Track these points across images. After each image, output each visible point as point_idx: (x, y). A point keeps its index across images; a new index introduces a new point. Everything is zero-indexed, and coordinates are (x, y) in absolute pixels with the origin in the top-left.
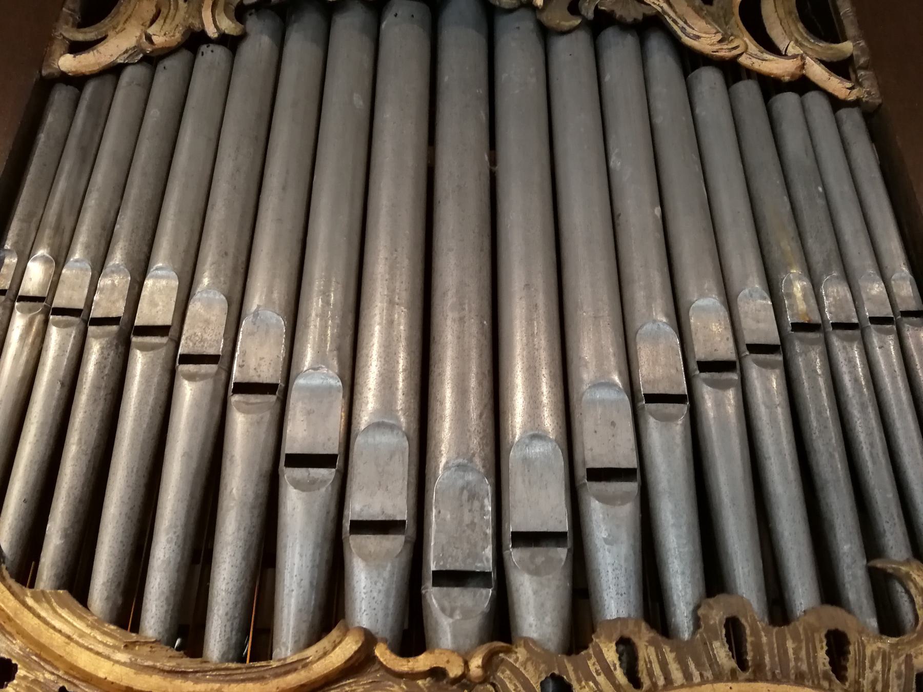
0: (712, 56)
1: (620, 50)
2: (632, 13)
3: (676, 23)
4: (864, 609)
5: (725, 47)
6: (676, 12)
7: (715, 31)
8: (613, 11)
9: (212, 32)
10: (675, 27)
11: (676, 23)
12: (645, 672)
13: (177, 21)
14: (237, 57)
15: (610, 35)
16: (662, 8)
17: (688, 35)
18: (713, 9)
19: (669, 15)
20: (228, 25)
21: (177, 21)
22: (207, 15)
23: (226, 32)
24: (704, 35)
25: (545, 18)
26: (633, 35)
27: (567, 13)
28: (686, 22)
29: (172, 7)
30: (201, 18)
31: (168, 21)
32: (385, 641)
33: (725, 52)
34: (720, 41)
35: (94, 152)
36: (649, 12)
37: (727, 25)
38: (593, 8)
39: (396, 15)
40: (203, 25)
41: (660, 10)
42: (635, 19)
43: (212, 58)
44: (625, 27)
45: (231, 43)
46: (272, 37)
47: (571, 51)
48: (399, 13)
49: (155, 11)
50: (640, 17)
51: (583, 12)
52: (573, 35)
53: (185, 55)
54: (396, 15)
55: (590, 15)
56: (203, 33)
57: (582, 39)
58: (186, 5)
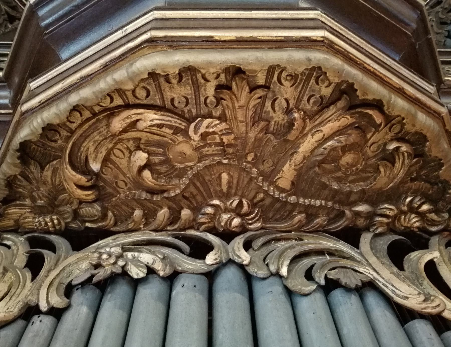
0: (422, 312)
1: (347, 305)
2: (352, 281)
3: (387, 287)
4: (151, 122)
5: (430, 305)
6: (383, 278)
7: (417, 293)
8: (339, 279)
9: (44, 307)
10: (386, 290)
11: (387, 287)
12: (129, 114)
13: (19, 299)
14: (60, 323)
15: (338, 295)
16: (372, 275)
17: (398, 296)
18: (407, 273)
19: (379, 281)
20: (57, 301)
21: (19, 299)
22: (43, 292)
23: (55, 306)
24: (410, 296)
25: (290, 284)
26: (355, 295)
27: (305, 280)
28: (393, 286)
29: (20, 287)
30: (38, 295)
31: (13, 298)
32: (112, 76)
33: (430, 308)
34: (424, 301)
35: (145, 11)
36: (365, 280)
37: (422, 286)
38: (323, 277)
39: (183, 286)
40: (38, 301)
41: (372, 277)
42: (356, 285)
43: (41, 325)
44: (348, 289)
45: (57, 313)
46: (90, 308)
47: (312, 308)
48: (185, 285)
49: (6, 290)
50: (360, 284)
51: (317, 280)
52: (312, 296)
53: (21, 323)
54: (183, 286)
55: (323, 282)
56: (37, 306)
57: (319, 297)
58: (31, 284)
